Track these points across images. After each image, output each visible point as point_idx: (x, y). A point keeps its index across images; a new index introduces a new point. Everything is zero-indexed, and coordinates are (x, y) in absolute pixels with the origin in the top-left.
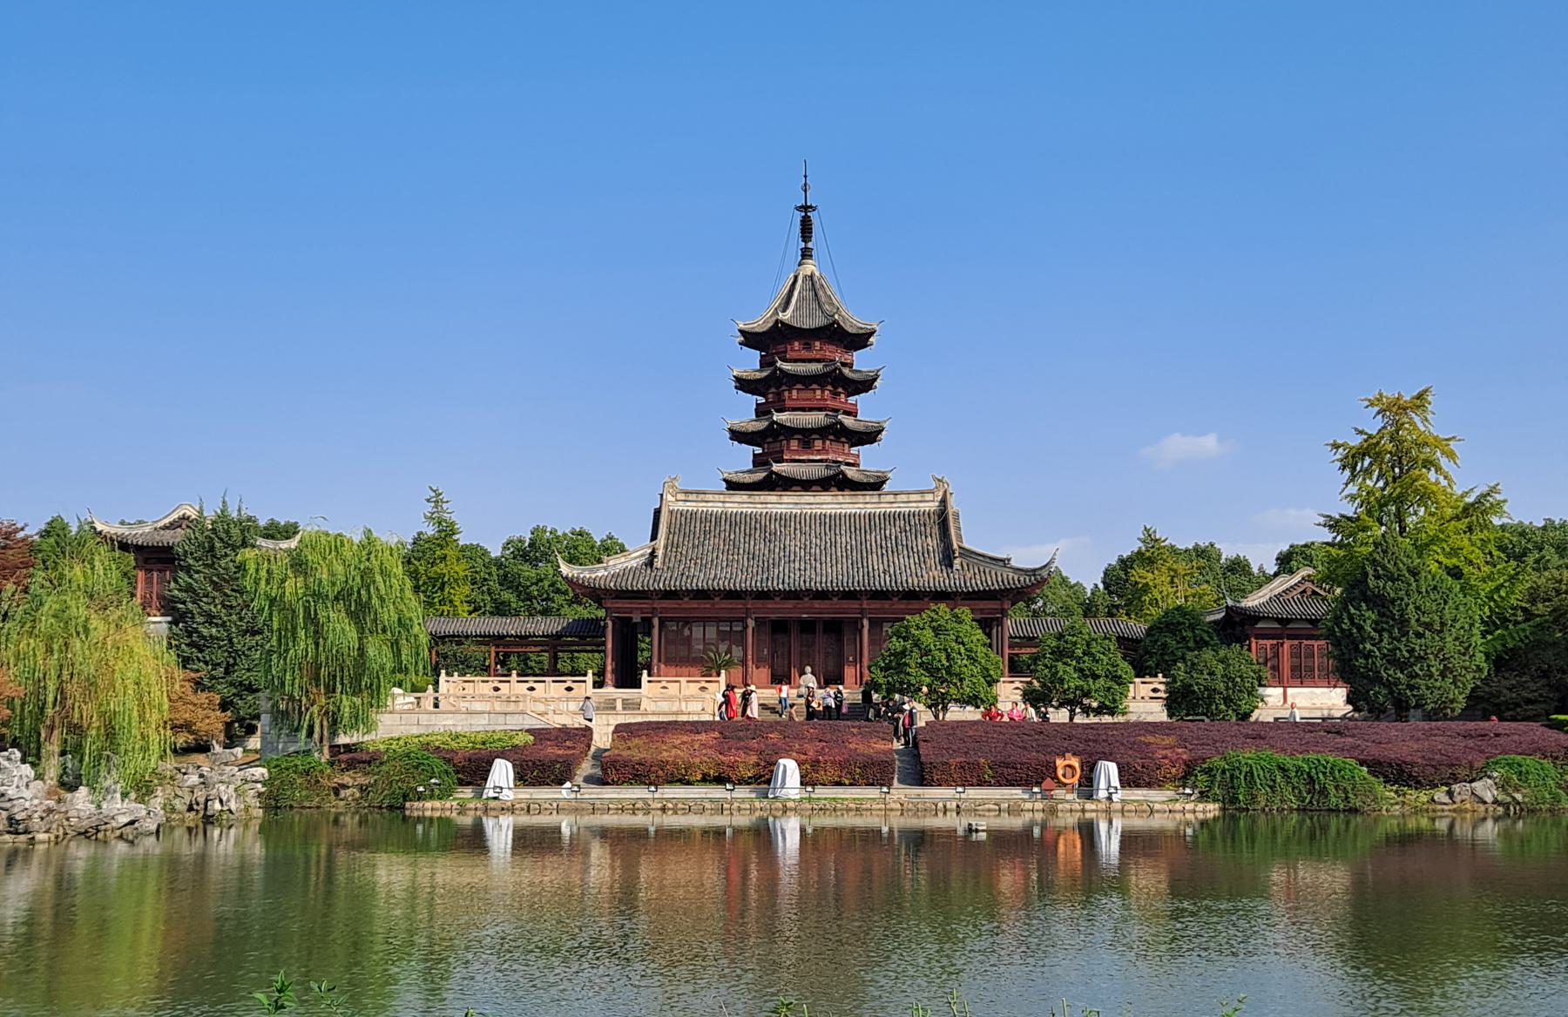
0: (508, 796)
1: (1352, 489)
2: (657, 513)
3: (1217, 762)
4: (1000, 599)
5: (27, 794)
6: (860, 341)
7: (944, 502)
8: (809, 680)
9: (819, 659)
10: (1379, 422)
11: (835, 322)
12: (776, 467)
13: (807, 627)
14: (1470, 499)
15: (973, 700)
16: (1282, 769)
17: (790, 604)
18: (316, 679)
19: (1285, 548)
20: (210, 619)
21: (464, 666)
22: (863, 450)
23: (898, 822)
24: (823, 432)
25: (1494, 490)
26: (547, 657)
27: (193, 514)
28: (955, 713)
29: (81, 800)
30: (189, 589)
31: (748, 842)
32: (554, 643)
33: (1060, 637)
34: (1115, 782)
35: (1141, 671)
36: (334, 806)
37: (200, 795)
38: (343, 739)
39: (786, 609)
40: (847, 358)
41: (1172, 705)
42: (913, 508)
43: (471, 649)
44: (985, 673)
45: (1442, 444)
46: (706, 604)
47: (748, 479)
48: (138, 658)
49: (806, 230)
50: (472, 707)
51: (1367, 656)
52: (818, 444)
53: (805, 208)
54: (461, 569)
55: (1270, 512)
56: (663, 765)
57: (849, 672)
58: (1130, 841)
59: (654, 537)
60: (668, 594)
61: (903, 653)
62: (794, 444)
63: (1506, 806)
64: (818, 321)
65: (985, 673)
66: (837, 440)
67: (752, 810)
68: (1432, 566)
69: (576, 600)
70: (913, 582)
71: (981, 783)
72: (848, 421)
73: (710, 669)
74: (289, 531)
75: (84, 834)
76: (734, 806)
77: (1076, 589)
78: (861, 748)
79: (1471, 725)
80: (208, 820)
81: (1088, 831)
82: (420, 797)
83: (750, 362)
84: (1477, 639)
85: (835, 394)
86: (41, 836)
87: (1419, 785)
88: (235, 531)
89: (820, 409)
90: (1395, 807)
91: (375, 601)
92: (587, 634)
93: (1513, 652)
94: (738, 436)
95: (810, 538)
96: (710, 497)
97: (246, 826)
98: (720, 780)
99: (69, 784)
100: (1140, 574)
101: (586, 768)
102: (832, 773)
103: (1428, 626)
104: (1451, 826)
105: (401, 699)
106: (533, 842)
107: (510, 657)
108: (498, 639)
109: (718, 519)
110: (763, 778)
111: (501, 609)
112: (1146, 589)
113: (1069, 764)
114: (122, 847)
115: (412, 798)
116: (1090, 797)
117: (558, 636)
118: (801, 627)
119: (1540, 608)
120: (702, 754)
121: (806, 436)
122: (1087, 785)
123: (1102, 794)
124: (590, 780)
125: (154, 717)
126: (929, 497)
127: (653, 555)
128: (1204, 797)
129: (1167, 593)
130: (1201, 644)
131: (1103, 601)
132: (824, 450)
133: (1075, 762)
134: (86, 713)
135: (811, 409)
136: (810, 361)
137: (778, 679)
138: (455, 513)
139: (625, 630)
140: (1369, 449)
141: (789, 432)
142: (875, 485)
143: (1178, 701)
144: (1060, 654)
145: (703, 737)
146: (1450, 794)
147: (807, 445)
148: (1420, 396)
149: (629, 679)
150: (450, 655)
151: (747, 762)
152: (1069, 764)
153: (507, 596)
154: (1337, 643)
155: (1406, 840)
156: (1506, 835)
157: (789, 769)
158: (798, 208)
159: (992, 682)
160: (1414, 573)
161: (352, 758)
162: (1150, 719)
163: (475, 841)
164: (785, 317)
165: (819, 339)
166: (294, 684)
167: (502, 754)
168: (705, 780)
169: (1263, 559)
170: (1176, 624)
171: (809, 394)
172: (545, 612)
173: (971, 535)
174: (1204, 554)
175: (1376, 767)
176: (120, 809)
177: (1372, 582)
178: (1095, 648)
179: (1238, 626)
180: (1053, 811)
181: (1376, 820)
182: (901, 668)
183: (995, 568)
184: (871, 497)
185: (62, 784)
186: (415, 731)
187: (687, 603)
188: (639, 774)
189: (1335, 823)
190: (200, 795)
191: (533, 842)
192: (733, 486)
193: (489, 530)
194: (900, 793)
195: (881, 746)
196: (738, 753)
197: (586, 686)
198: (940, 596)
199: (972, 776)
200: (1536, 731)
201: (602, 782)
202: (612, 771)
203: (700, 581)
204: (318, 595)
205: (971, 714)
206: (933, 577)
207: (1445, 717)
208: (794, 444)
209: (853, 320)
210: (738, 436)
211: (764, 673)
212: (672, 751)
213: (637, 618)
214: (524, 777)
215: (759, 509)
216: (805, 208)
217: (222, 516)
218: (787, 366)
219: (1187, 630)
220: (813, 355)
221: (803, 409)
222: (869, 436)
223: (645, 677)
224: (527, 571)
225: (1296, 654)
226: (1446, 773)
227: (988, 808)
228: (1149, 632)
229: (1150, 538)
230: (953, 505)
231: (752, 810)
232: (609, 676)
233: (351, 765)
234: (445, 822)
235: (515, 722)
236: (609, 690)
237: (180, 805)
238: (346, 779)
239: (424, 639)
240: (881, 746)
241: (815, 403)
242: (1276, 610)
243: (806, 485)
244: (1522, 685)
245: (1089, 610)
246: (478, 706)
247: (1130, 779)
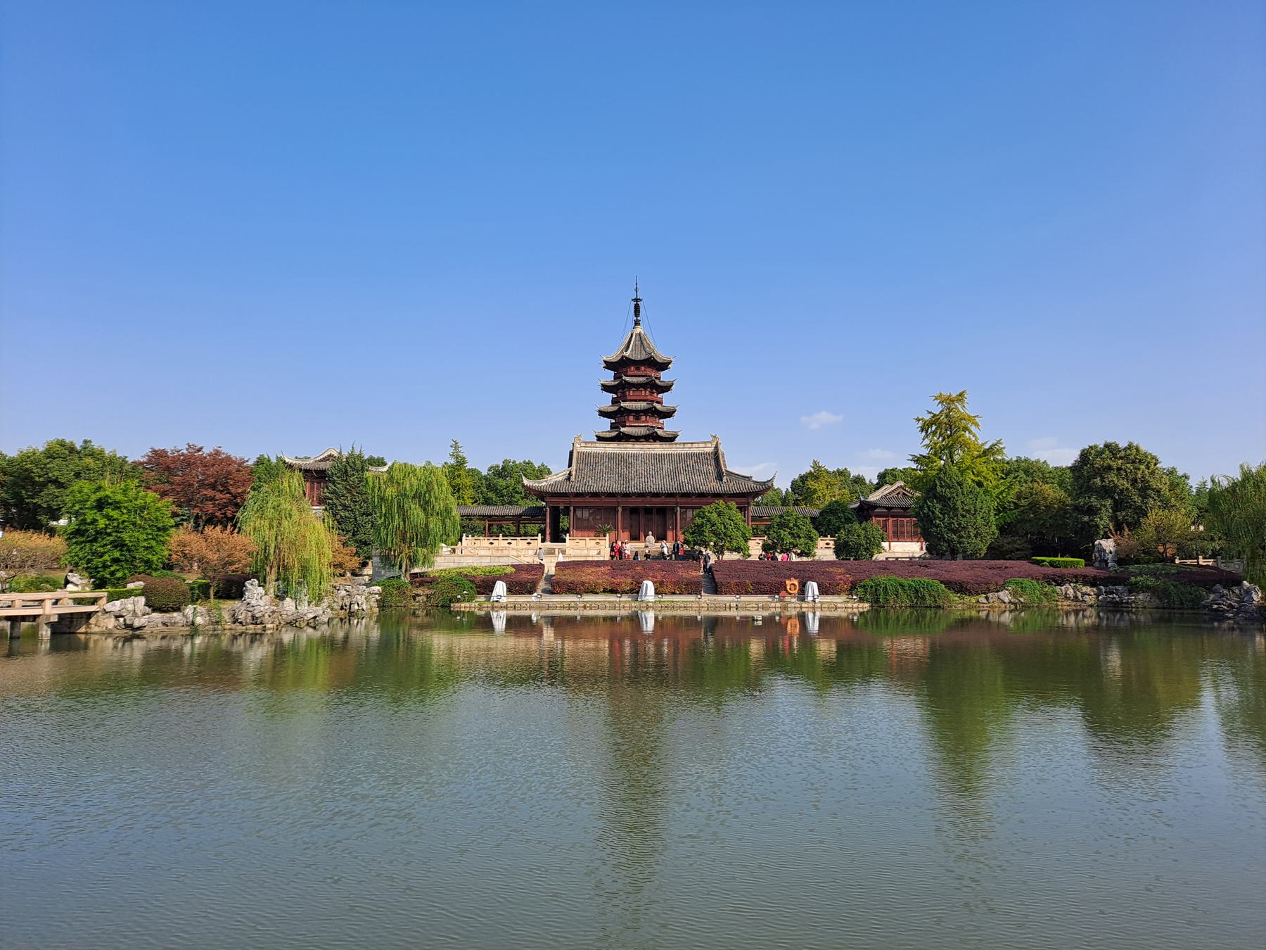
0: (504, 600)
1: (927, 441)
2: (571, 453)
3: (868, 582)
4: (747, 496)
5: (261, 603)
6: (664, 366)
7: (716, 447)
8: (651, 538)
9: (654, 528)
10: (940, 408)
12: (622, 430)
13: (648, 511)
14: (987, 447)
15: (738, 550)
16: (901, 585)
17: (640, 499)
18: (404, 540)
19: (882, 471)
20: (345, 508)
21: (473, 531)
22: (666, 421)
23: (705, 613)
25: (999, 442)
26: (516, 527)
27: (336, 455)
28: (728, 556)
29: (289, 603)
30: (334, 492)
31: (627, 626)
32: (517, 519)
33: (781, 517)
34: (817, 593)
35: (823, 534)
36: (414, 605)
37: (347, 602)
38: (416, 570)
39: (638, 502)
40: (657, 375)
41: (838, 551)
42: (701, 450)
43: (476, 523)
44: (744, 535)
45: (972, 420)
46: (597, 500)
47: (608, 435)
48: (314, 532)
49: (637, 311)
50: (478, 554)
51: (937, 527)
53: (637, 300)
54: (468, 481)
55: (880, 450)
56: (583, 584)
57: (670, 534)
58: (824, 622)
59: (570, 465)
60: (578, 495)
61: (702, 525)
62: (631, 418)
63: (1015, 604)
65: (744, 535)
67: (630, 607)
68: (969, 478)
69: (526, 497)
70: (703, 489)
71: (747, 593)
72: (658, 407)
73: (600, 533)
74: (381, 463)
75: (290, 623)
76: (621, 605)
77: (778, 491)
78: (685, 575)
79: (992, 562)
80: (351, 614)
81: (802, 617)
82: (458, 601)
84: (992, 518)
85: (652, 393)
86: (269, 626)
87: (970, 594)
88: (358, 462)
90: (959, 605)
91: (433, 499)
92: (535, 515)
93: (1009, 524)
94: (603, 414)
95: (644, 466)
97: (371, 618)
98: (613, 591)
99: (280, 597)
100: (811, 484)
101: (542, 585)
102: (671, 588)
103: (968, 511)
104: (988, 615)
105: (445, 549)
106: (518, 624)
107: (493, 527)
108: (489, 517)
109: (602, 456)
110: (635, 590)
111: (487, 502)
112: (815, 491)
113: (792, 584)
114: (310, 630)
115: (452, 602)
116: (803, 600)
117: (520, 516)
118: (646, 511)
119: (1023, 502)
120: (604, 581)
121: (637, 414)
122: (802, 592)
123: (810, 599)
124: (544, 591)
125: (325, 561)
127: (570, 474)
128: (861, 600)
129: (827, 495)
130: (848, 520)
131: (792, 497)
132: (646, 421)
134: (292, 559)
137: (635, 538)
138: (464, 453)
139: (553, 514)
140: (935, 421)
142: (671, 439)
143: (842, 549)
144: (781, 526)
145: (602, 569)
146: (987, 598)
147: (637, 418)
148: (961, 395)
149: (557, 537)
150: (470, 526)
151: (626, 582)
152: (792, 584)
153: (490, 495)
154: (921, 520)
155: (964, 623)
156: (1015, 619)
157: (649, 586)
159: (746, 540)
160: (960, 484)
161: (421, 580)
162: (825, 559)
163: (485, 624)
164: (627, 354)
166: (393, 541)
167: (500, 579)
168: (605, 591)
169: (871, 477)
170: (833, 510)
172: (510, 503)
173: (732, 465)
174: (842, 473)
175: (948, 584)
176: (307, 610)
177: (939, 489)
178: (799, 523)
179: (866, 511)
180: (786, 608)
181: (950, 612)
182: (701, 533)
183: (743, 482)
184: (665, 445)
185: (277, 596)
186: (452, 565)
187: (588, 499)
188: (571, 589)
189: (929, 613)
190: (347, 602)
192: (600, 439)
193: (481, 462)
194: (707, 598)
195: (694, 574)
196: (622, 575)
197: (537, 543)
198: (717, 495)
199: (742, 590)
200: (1025, 565)
201: (552, 593)
202: (556, 587)
203: (594, 489)
205: (735, 556)
206: (712, 486)
207: (977, 558)
208: (631, 418)
209: (661, 356)
210: (603, 414)
211: (627, 534)
212: (587, 576)
213: (562, 507)
214: (511, 591)
215: (623, 451)
216: (637, 300)
217: (351, 455)
218: (628, 379)
219: (844, 514)
222: (669, 414)
223: (567, 537)
224: (501, 482)
225: (895, 525)
226: (985, 588)
227: (756, 606)
228: (821, 514)
229: (816, 465)
230: (721, 448)
231: (630, 607)
232: (548, 537)
233: (421, 584)
234: (471, 613)
235: (504, 561)
236: (548, 544)
237: (336, 606)
238: (420, 591)
239: (458, 518)
240: (694, 574)
242: (885, 503)
243: (637, 439)
244: (1015, 542)
245: (784, 502)
246: (482, 553)
247: (824, 591)
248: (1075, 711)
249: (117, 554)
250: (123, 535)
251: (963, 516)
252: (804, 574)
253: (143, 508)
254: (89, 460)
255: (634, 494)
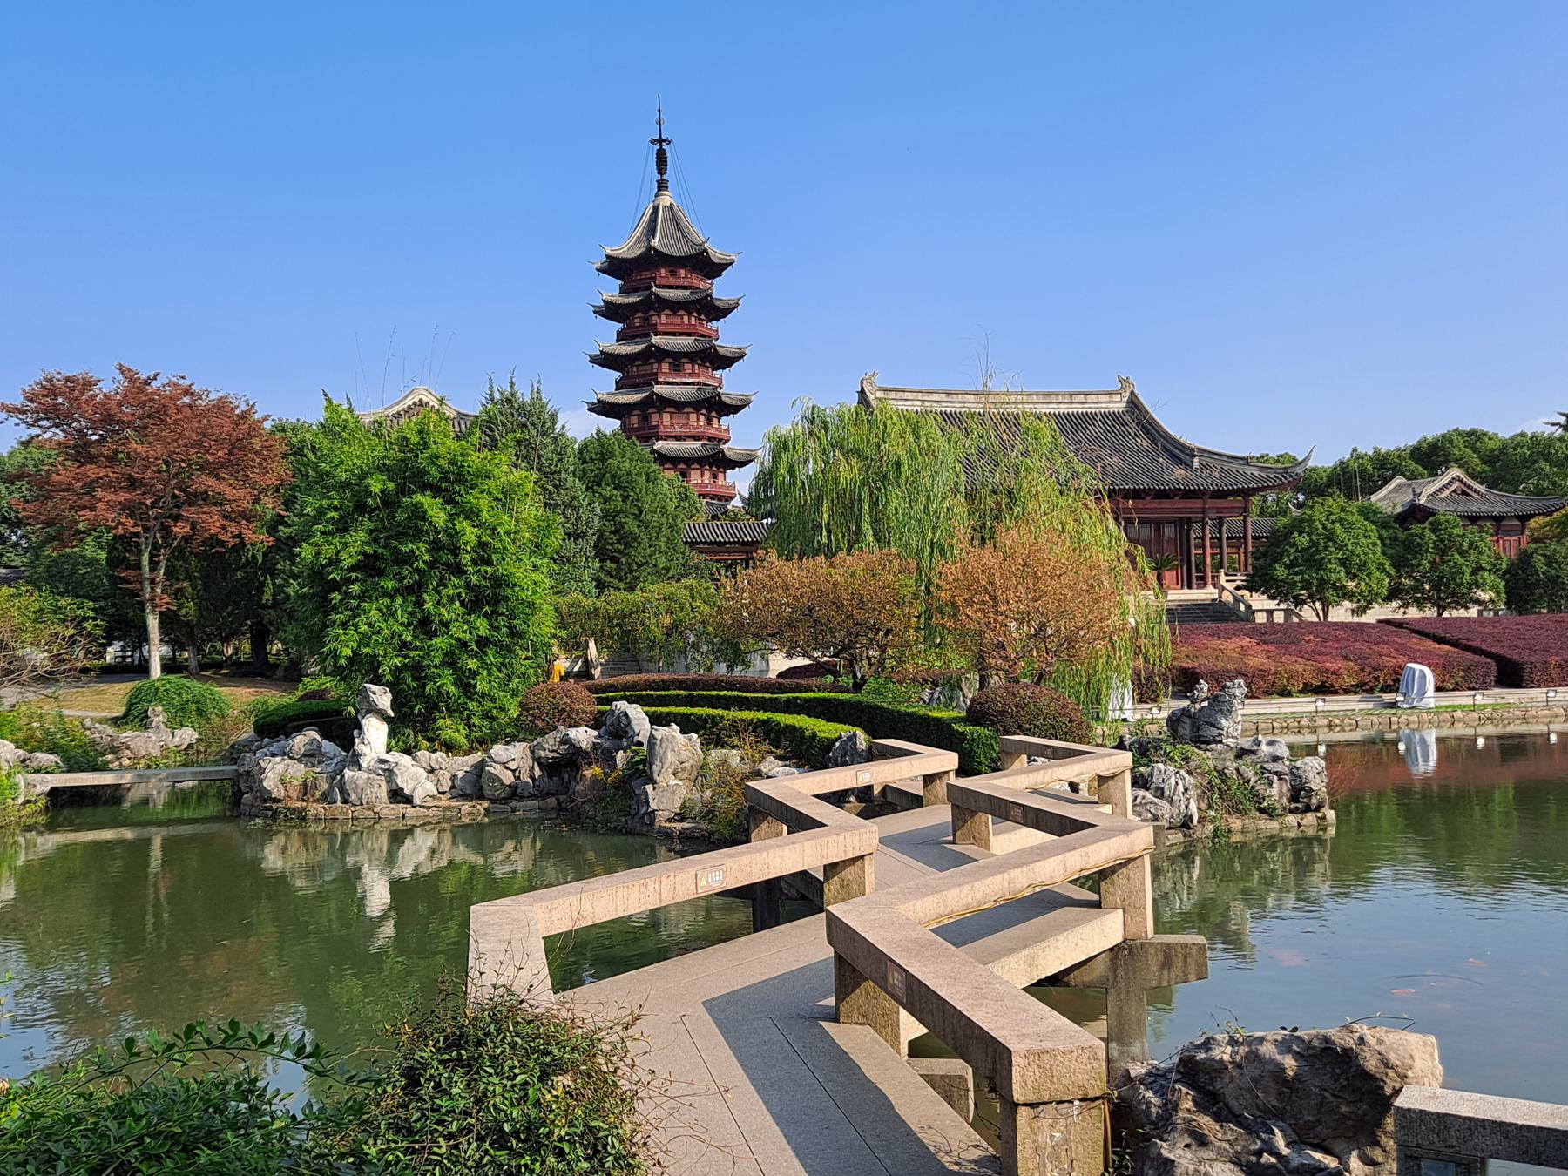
6: (712, 269)
11: (705, 251)
24: (692, 356)
52: (688, 367)
53: (660, 141)
62: (665, 367)
89: (689, 334)
96: (909, 396)
98: (1323, 690)
121: (677, 359)
126: (1117, 398)
135: (681, 334)
136: (678, 287)
141: (662, 354)
147: (677, 368)
158: (654, 142)
165: (684, 267)
168: (1307, 690)
171: (678, 320)
208: (665, 367)
209: (716, 253)
216: (660, 141)
220: (680, 282)
221: (673, 334)
241: (685, 329)
248: (584, 745)
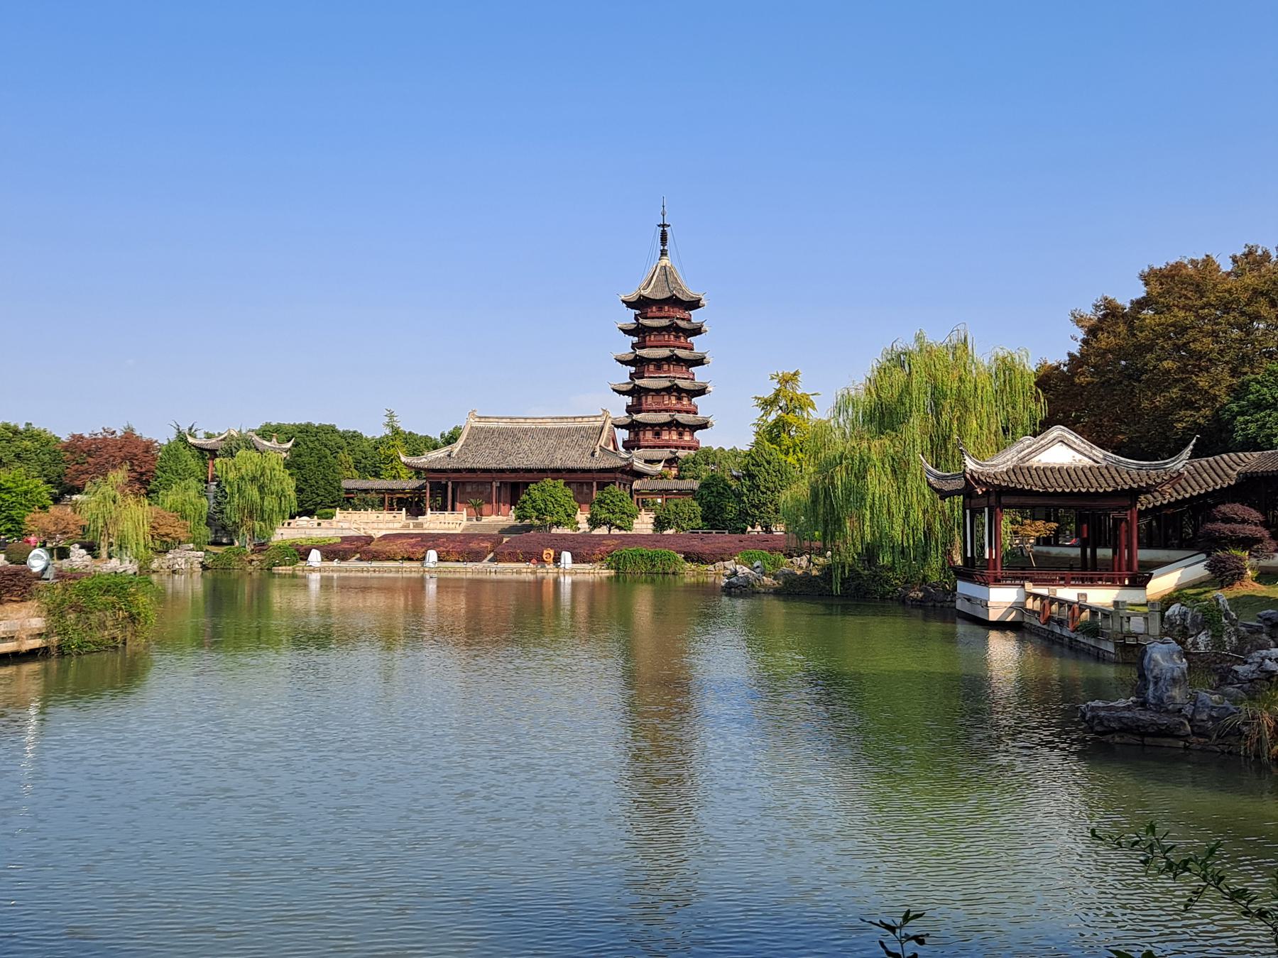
6: (695, 304)
17: (513, 475)
36: (250, 568)
42: (591, 424)
46: (474, 475)
52: (666, 367)
60: (458, 471)
62: (652, 367)
64: (666, 295)
66: (678, 364)
71: (518, 561)
81: (557, 583)
83: (628, 317)
85: (677, 337)
98: (410, 559)
113: (549, 553)
121: (659, 363)
122: (557, 560)
133: (552, 553)
164: (645, 293)
168: (403, 559)
171: (659, 338)
191: (326, 584)
204: (242, 478)
208: (652, 367)
209: (690, 290)
220: (662, 314)
238: (254, 557)
249: (9, 526)
250: (13, 512)
251: (763, 493)
252: (560, 544)
253: (26, 493)
254: (27, 443)
255: (479, 470)
